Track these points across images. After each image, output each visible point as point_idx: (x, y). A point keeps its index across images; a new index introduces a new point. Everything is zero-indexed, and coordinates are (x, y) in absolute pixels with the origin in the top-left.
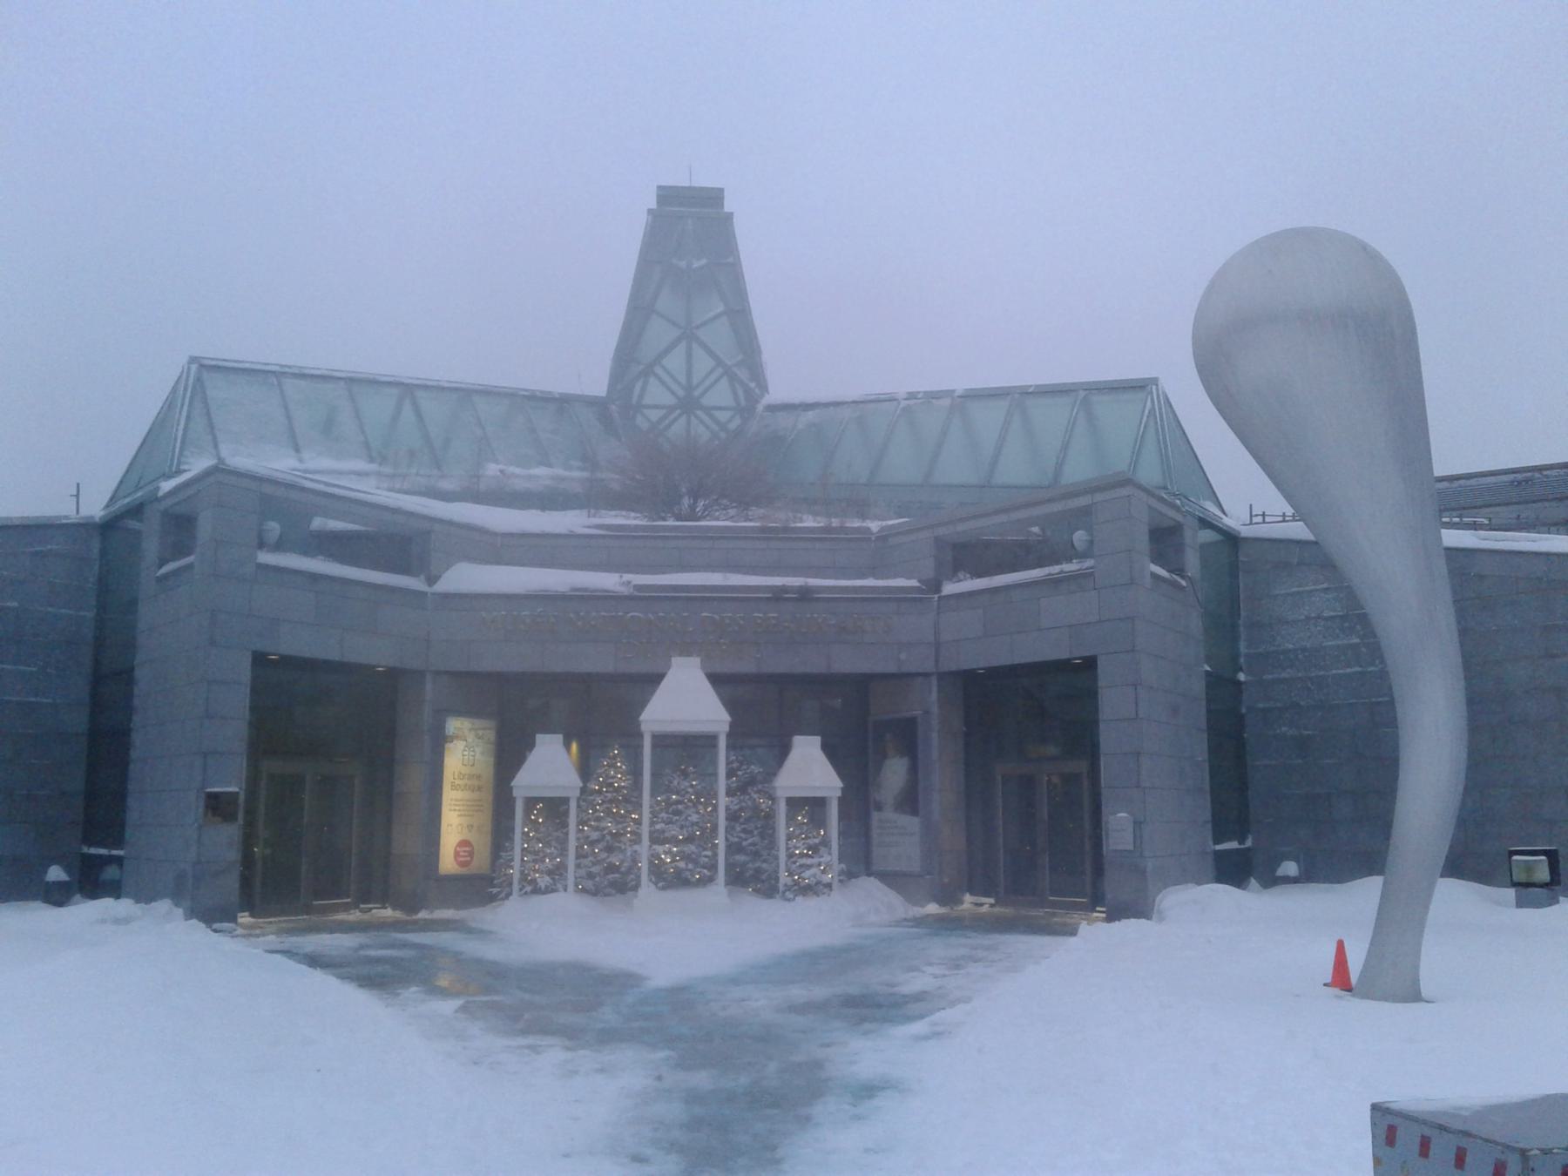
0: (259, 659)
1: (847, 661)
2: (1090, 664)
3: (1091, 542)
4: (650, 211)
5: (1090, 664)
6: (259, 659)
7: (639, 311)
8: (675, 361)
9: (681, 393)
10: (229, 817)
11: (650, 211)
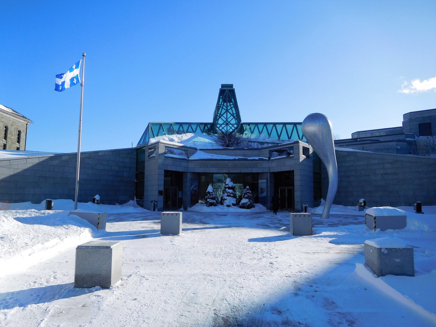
0: (165, 170)
1: (255, 171)
2: (293, 171)
3: (293, 152)
4: (220, 89)
5: (293, 171)
6: (165, 170)
7: (218, 107)
8: (225, 115)
9: (225, 120)
10: (162, 194)
11: (220, 89)
